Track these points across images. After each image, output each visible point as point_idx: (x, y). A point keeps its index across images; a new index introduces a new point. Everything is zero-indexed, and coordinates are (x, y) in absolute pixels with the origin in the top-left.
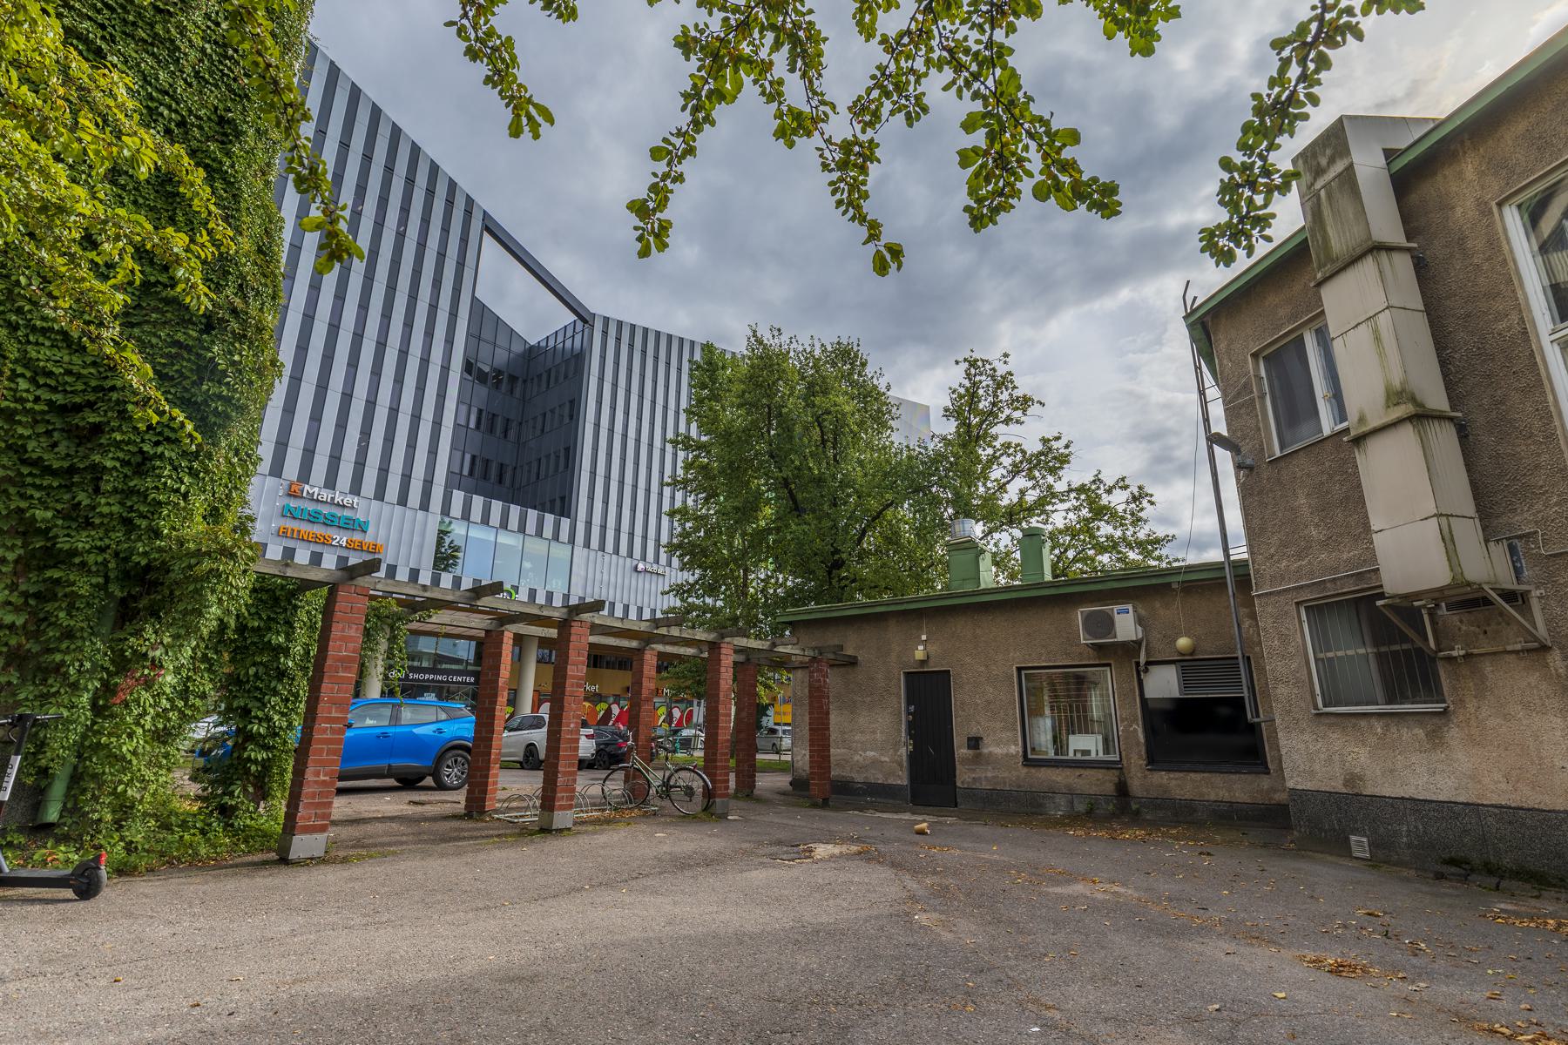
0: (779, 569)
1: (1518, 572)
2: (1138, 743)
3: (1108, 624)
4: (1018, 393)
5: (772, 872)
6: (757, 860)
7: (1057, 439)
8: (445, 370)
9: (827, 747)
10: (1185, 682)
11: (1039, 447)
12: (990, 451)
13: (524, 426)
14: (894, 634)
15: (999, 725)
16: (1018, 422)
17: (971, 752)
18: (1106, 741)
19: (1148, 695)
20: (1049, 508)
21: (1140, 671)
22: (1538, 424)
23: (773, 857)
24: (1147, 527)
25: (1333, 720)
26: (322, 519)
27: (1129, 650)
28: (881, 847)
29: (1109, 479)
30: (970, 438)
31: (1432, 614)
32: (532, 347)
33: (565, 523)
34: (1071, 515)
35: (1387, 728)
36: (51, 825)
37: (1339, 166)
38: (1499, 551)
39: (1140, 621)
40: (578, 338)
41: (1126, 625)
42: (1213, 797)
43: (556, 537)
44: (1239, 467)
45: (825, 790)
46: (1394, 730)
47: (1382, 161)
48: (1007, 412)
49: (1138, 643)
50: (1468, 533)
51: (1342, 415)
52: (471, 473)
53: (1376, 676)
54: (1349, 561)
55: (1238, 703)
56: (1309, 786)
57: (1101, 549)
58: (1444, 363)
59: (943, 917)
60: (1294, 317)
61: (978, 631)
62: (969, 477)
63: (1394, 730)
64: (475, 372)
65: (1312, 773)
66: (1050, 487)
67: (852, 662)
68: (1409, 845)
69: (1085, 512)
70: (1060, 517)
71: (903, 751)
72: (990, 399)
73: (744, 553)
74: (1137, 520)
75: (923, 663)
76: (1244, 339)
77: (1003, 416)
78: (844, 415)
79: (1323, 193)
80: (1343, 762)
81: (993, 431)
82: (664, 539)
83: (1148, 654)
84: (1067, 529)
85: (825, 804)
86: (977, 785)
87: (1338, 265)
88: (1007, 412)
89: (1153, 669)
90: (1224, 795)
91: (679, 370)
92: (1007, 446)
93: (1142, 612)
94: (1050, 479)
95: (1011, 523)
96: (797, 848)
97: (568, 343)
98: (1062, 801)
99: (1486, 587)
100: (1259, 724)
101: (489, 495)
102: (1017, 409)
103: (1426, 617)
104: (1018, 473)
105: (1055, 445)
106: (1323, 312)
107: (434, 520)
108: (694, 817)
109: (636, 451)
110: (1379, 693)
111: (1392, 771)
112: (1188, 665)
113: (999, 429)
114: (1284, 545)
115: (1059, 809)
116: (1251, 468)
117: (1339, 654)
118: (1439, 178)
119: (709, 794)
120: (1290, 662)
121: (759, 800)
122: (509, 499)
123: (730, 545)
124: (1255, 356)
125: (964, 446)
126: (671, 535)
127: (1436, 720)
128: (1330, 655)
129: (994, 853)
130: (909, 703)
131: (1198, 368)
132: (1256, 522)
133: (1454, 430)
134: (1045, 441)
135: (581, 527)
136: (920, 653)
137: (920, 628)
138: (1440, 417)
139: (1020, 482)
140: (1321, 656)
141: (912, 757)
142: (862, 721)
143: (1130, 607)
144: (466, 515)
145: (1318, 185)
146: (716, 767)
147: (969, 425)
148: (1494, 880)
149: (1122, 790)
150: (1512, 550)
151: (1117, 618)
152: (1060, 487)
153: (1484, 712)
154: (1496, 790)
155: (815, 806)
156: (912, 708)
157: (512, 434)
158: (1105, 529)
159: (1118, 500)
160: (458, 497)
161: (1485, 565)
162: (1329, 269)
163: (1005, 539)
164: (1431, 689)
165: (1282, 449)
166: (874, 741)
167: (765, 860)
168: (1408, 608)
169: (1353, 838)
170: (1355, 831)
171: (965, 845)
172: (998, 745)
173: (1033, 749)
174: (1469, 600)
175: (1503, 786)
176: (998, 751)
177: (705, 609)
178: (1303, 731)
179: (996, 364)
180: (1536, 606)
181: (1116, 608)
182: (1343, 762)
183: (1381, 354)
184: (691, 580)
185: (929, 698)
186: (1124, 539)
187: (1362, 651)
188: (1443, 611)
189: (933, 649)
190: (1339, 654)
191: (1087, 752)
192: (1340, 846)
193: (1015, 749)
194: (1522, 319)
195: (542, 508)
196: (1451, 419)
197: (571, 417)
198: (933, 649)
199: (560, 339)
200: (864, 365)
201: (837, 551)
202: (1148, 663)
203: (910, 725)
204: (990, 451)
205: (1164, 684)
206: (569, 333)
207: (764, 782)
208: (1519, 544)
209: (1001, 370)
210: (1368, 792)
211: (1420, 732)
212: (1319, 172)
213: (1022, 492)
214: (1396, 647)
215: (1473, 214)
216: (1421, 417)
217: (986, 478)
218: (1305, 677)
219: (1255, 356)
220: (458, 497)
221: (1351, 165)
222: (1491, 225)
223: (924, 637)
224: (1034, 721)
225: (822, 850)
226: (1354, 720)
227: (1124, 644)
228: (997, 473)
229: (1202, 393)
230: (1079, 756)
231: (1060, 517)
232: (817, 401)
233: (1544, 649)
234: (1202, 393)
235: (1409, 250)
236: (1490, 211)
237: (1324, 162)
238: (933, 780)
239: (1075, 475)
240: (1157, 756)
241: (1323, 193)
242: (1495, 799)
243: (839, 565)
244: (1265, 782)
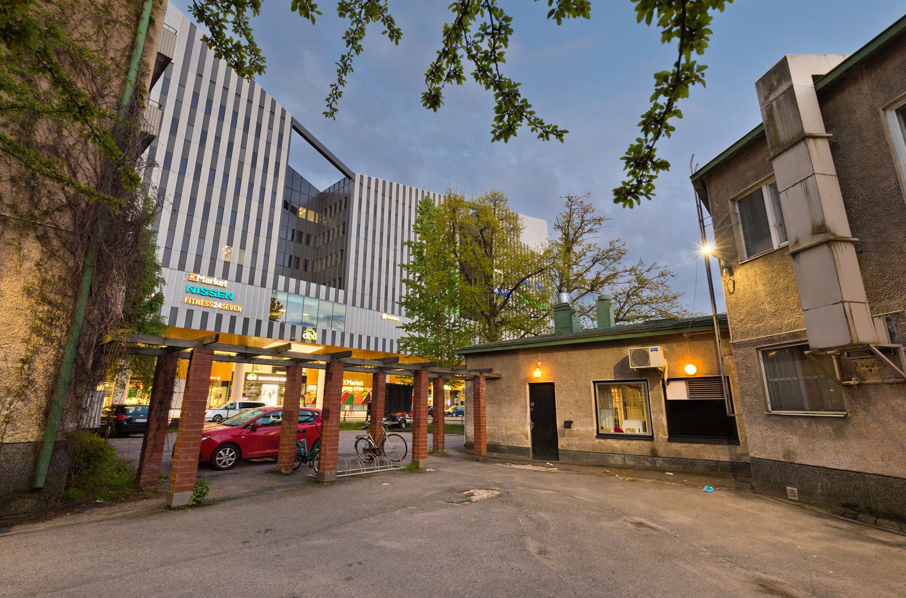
1: (892, 335)
2: (663, 426)
5: (445, 511)
8: (273, 206)
10: (691, 391)
13: (315, 244)
15: (582, 414)
19: (668, 398)
25: (777, 418)
26: (207, 293)
30: (569, 242)
32: (321, 194)
33: (341, 292)
36: (40, 489)
37: (784, 87)
38: (880, 324)
40: (346, 187)
42: (706, 458)
43: (336, 300)
46: (814, 426)
47: (811, 82)
51: (784, 236)
52: (290, 266)
54: (788, 324)
55: (722, 403)
56: (763, 456)
58: (848, 207)
60: (756, 177)
63: (814, 426)
64: (289, 207)
65: (765, 449)
68: (822, 495)
76: (726, 191)
77: (587, 228)
79: (774, 103)
82: (397, 299)
85: (485, 461)
86: (570, 449)
89: (672, 384)
97: (341, 190)
99: (872, 346)
100: (734, 417)
101: (299, 278)
103: (835, 361)
107: (267, 293)
109: (381, 245)
113: (584, 236)
117: (782, 379)
118: (846, 93)
122: (310, 280)
126: (401, 297)
127: (840, 422)
128: (776, 380)
130: (531, 401)
131: (699, 207)
133: (853, 249)
135: (350, 294)
138: (845, 241)
139: (598, 267)
140: (771, 380)
142: (504, 410)
144: (286, 289)
148: (874, 518)
152: (620, 268)
154: (874, 465)
157: (311, 244)
160: (282, 279)
163: (590, 301)
169: (788, 488)
172: (582, 426)
176: (582, 429)
178: (759, 424)
181: (650, 348)
185: (543, 398)
190: (782, 379)
191: (633, 430)
194: (897, 182)
195: (328, 284)
196: (852, 242)
197: (344, 233)
199: (336, 188)
205: (678, 392)
206: (342, 185)
210: (798, 461)
212: (772, 89)
218: (761, 393)
219: (733, 200)
220: (282, 279)
222: (879, 122)
224: (603, 411)
226: (790, 419)
229: (701, 221)
231: (623, 284)
234: (701, 221)
236: (878, 114)
240: (677, 432)
241: (774, 103)
242: (875, 470)
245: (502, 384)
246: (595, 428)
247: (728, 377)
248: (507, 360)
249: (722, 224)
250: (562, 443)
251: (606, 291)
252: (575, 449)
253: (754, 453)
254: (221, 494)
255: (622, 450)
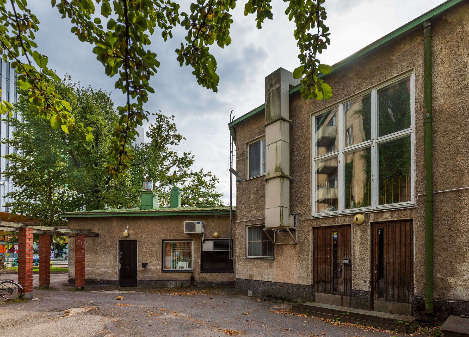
0: (70, 188)
1: (295, 223)
2: (199, 265)
3: (194, 227)
4: (177, 133)
5: (46, 325)
6: (40, 320)
7: (190, 154)
9: (83, 268)
10: (215, 246)
11: (182, 156)
12: (165, 154)
14: (115, 225)
15: (154, 259)
16: (176, 144)
17: (143, 268)
18: (190, 264)
20: (185, 179)
21: (202, 242)
22: (307, 184)
23: (49, 317)
24: (216, 190)
25: (249, 260)
27: (199, 236)
28: (101, 307)
29: (205, 173)
31: (276, 233)
34: (192, 183)
35: (261, 262)
39: (204, 226)
41: (199, 228)
42: (218, 280)
44: (237, 181)
45: (82, 283)
47: (288, 89)
48: (172, 140)
49: (202, 234)
50: (286, 211)
53: (261, 248)
56: (241, 278)
57: (201, 196)
58: (291, 160)
59: (116, 334)
61: (149, 226)
62: (156, 164)
65: (242, 274)
66: (185, 172)
67: (97, 235)
68: (260, 292)
69: (196, 182)
70: (188, 182)
71: (117, 269)
72: (166, 133)
73: (49, 180)
74: (213, 187)
75: (126, 237)
76: (246, 135)
77: (170, 141)
78: (101, 126)
79: (271, 93)
80: (250, 271)
81: (167, 146)
83: (205, 237)
84: (190, 187)
85: (82, 289)
86: (145, 279)
87: (271, 121)
88: (172, 140)
89: (206, 242)
90: (221, 279)
91: (8, 79)
92: (171, 153)
93: (205, 223)
94: (185, 169)
95: (170, 183)
96: (62, 310)
98: (173, 283)
102: (176, 139)
104: (174, 164)
105: (189, 156)
106: (265, 135)
108: (13, 301)
110: (261, 253)
111: (260, 274)
112: (217, 241)
113: (168, 146)
114: (245, 208)
115: (172, 285)
116: (240, 182)
117: (254, 241)
119: (21, 292)
120: (243, 240)
121: (52, 289)
123: (42, 177)
124: (247, 144)
125: (154, 150)
127: (272, 261)
128: (252, 241)
129: (144, 305)
130: (120, 251)
131: (231, 143)
132: (239, 199)
134: (185, 154)
136: (125, 233)
137: (126, 224)
138: (287, 177)
139: (175, 168)
140: (249, 242)
141: (121, 270)
142: (100, 257)
143: (201, 222)
145: (271, 90)
146: (25, 280)
147: (157, 141)
148: (275, 300)
149: (192, 279)
150: (295, 217)
151: (197, 225)
152: (189, 172)
153: (282, 259)
154: (280, 279)
155: (77, 290)
156: (121, 253)
158: (202, 189)
159: (207, 179)
161: (289, 222)
162: (269, 121)
163: (167, 189)
164: (272, 253)
165: (250, 177)
166: (105, 264)
167: (45, 319)
168: (270, 231)
170: (250, 289)
171: (135, 302)
172: (153, 266)
173: (165, 267)
174: (283, 230)
175: (282, 278)
176: (153, 268)
177: (28, 205)
179: (169, 119)
180: (297, 232)
181: (197, 222)
182: (250, 271)
183: (276, 154)
184: (21, 190)
185: (128, 250)
186: (208, 193)
187: (259, 241)
188: (278, 232)
189: (131, 232)
191: (183, 267)
192: (246, 293)
193: (159, 267)
196: (289, 178)
198: (131, 232)
200: (112, 104)
201: (96, 186)
202: (205, 240)
203: (121, 259)
204: (165, 154)
205: (209, 246)
207: (55, 279)
208: (297, 216)
209: (171, 122)
211: (268, 264)
212: (272, 86)
213: (175, 172)
214: (267, 241)
215: (306, 115)
216: (282, 177)
217: (162, 164)
219: (247, 144)
221: (280, 87)
223: (128, 227)
225: (74, 311)
227: (197, 234)
228: (166, 163)
230: (180, 269)
231: (188, 182)
232: (88, 116)
233: (296, 244)
235: (289, 122)
237: (273, 83)
238: (128, 277)
239: (193, 169)
241: (271, 93)
243: (97, 191)
244: (232, 275)
245: (99, 240)
246: (161, 267)
247: (233, 240)
248: (104, 224)
249: (240, 157)
250: (140, 276)
251: (179, 185)
252: (148, 279)
253: (238, 276)
254: (186, 274)
255: (176, 279)
